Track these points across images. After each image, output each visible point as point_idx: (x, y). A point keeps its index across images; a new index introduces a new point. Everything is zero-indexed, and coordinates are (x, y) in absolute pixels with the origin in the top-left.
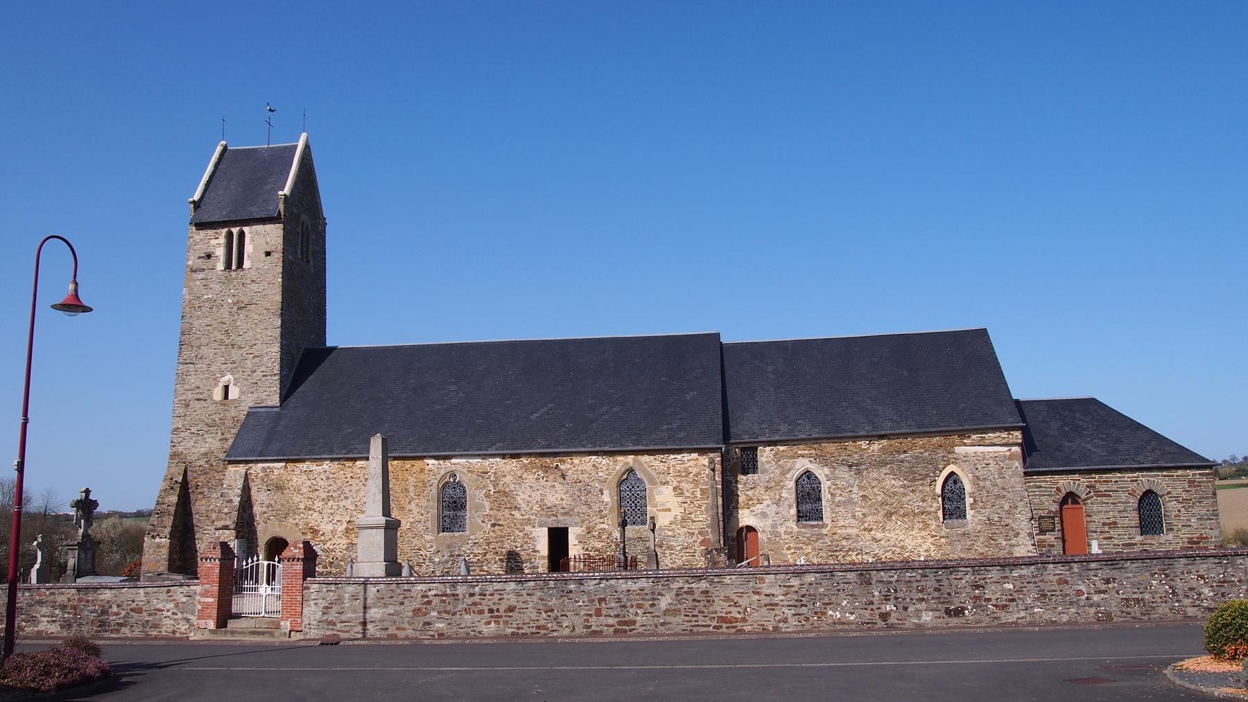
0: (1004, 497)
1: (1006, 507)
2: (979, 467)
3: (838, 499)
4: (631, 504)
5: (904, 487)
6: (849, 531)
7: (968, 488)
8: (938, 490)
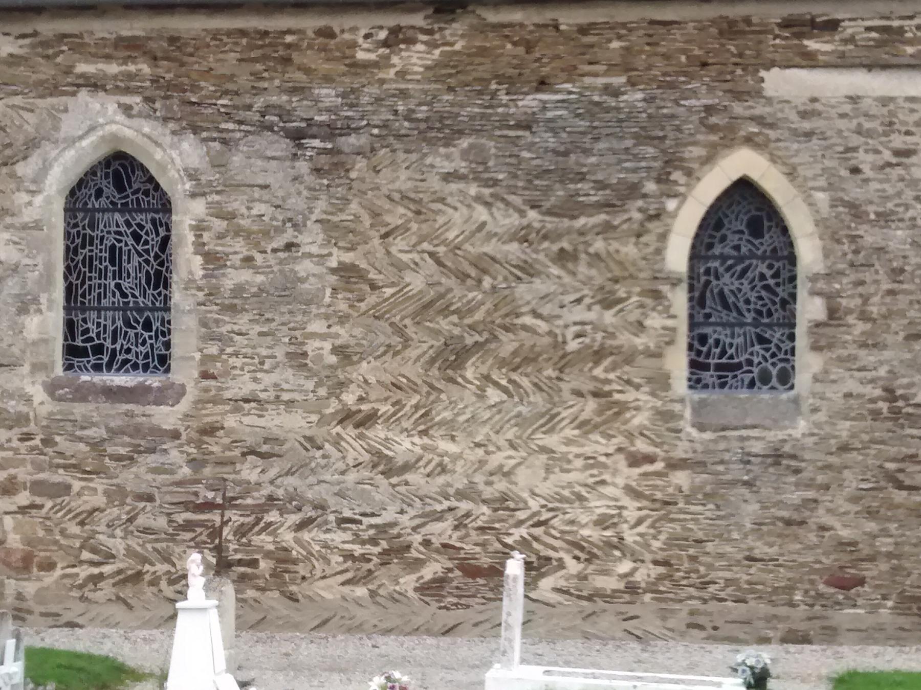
2: (865, 160)
3: (233, 277)
5: (523, 236)
6: (276, 421)
7: (809, 252)
8: (677, 256)
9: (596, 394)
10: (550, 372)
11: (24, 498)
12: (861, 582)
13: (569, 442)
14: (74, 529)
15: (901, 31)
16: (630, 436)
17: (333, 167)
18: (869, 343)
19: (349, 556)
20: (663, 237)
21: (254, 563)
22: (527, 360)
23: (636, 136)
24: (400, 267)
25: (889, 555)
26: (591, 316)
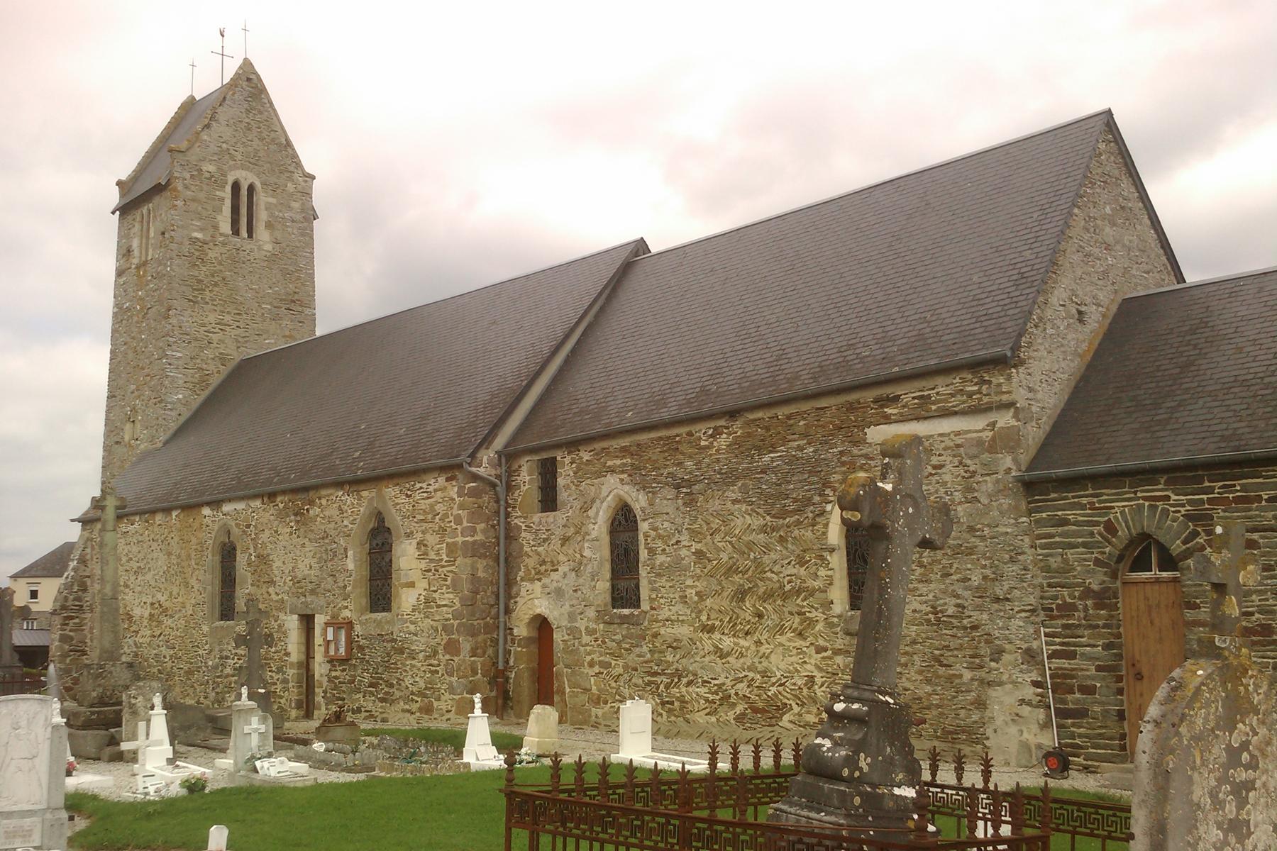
0: (971, 551)
1: (976, 580)
3: (660, 559)
4: (507, 745)
5: (763, 529)
9: (799, 614)
10: (779, 602)
11: (597, 669)
12: (924, 722)
13: (790, 640)
14: (614, 684)
15: (929, 397)
16: (816, 637)
17: (691, 501)
18: (924, 580)
19: (707, 700)
20: (826, 526)
21: (672, 703)
22: (771, 596)
23: (810, 472)
24: (718, 550)
25: (938, 706)
26: (794, 571)
